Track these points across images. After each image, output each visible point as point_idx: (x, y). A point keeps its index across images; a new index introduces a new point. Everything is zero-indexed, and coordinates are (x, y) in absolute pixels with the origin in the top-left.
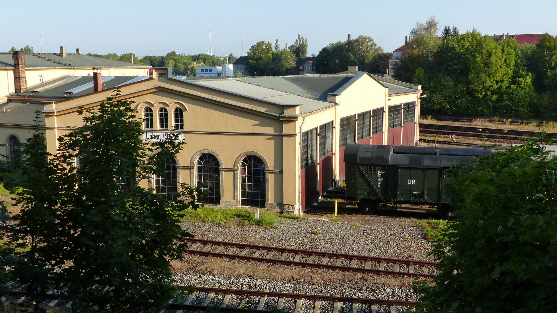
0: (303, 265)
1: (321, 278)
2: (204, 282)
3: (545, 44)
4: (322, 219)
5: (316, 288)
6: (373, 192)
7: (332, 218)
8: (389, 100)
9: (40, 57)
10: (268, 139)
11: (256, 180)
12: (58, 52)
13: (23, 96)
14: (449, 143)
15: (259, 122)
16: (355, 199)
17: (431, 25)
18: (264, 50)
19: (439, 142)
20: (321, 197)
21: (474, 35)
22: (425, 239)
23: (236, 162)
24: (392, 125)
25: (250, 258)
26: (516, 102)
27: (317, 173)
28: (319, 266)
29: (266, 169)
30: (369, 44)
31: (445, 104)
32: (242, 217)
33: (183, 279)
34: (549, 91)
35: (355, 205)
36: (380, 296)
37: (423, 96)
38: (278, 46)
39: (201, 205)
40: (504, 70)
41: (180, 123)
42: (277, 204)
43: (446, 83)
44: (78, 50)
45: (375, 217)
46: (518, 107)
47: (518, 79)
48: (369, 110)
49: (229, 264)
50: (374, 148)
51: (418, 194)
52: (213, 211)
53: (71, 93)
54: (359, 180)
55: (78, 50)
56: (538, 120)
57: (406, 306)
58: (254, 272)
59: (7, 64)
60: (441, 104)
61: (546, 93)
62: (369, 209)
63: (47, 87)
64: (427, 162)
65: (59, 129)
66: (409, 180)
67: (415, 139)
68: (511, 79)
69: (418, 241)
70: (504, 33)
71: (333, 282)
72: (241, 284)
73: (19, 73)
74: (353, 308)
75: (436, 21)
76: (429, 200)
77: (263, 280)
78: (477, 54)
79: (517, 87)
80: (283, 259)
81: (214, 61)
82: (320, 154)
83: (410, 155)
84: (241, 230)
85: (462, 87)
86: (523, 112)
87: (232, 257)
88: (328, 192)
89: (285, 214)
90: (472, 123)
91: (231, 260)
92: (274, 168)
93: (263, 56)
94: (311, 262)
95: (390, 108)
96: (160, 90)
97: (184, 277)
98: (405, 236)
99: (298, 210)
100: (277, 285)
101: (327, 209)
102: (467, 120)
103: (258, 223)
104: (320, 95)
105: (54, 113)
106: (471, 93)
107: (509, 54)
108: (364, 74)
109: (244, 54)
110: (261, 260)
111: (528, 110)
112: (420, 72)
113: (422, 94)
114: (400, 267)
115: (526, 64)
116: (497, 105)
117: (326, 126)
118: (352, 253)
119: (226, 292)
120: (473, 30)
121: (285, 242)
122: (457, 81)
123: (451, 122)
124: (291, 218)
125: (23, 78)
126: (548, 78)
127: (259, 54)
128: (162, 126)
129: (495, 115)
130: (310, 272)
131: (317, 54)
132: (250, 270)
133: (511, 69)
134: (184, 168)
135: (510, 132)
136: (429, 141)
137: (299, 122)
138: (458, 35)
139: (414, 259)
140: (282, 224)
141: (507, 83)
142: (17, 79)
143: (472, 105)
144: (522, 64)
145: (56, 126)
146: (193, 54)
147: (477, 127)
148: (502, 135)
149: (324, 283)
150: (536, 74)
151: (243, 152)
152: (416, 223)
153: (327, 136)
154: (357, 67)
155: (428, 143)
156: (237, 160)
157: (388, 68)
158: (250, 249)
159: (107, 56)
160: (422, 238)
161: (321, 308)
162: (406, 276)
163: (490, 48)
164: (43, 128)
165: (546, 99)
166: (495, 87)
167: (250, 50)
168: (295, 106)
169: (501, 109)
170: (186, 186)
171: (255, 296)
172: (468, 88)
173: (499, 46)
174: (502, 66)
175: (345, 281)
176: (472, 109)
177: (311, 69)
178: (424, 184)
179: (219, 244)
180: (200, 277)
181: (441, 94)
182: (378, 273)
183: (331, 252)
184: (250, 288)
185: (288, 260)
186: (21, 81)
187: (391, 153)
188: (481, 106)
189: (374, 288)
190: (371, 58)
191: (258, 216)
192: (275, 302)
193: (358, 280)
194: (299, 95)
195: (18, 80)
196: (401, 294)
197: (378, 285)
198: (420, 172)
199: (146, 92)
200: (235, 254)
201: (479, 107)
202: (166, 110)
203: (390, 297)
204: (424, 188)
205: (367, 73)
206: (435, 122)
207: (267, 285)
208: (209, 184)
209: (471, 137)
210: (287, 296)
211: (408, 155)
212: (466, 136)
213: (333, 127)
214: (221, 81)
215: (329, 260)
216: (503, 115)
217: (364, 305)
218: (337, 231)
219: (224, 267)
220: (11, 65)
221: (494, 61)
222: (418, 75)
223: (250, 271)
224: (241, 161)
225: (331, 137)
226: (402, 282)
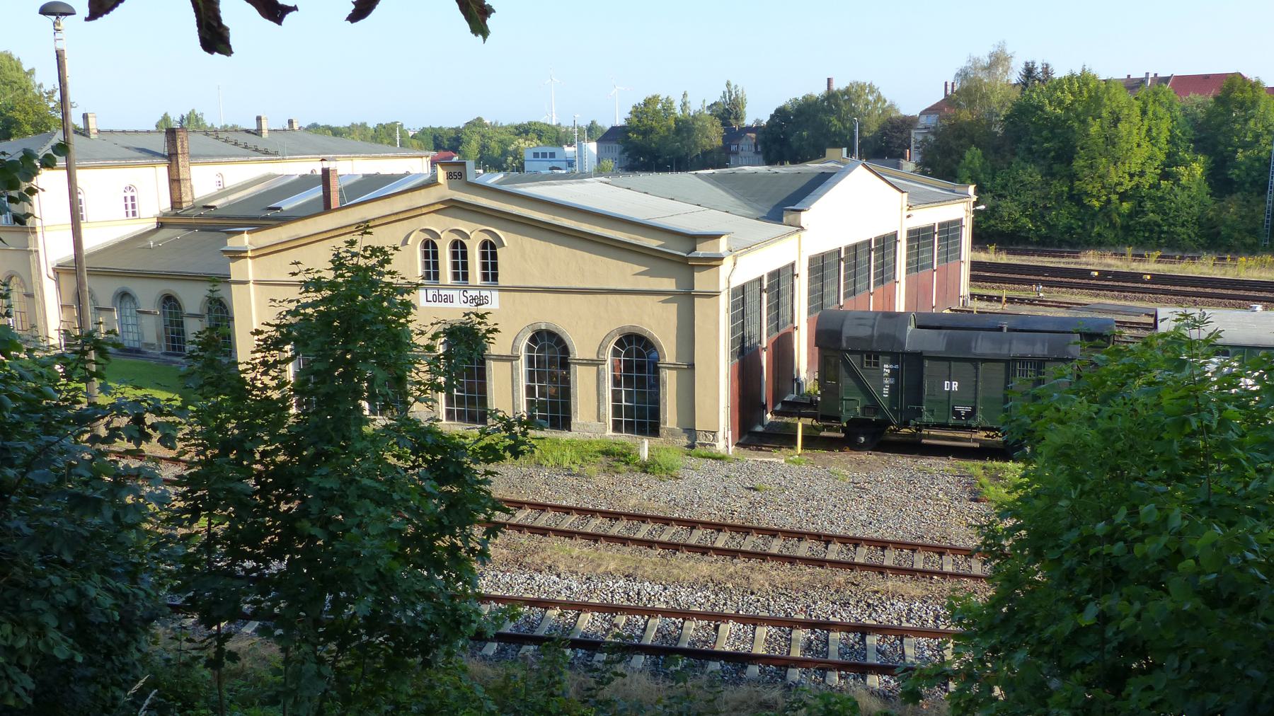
0: (733, 554)
1: (767, 581)
2: (539, 587)
3: (1232, 95)
4: (772, 460)
5: (758, 601)
6: (874, 406)
7: (791, 458)
8: (909, 216)
9: (217, 138)
10: (664, 302)
11: (641, 382)
12: (253, 126)
13: (186, 215)
14: (1031, 302)
16: (838, 419)
17: (998, 60)
18: (659, 112)
19: (1010, 300)
21: (1084, 79)
22: (976, 500)
23: (602, 347)
24: (913, 266)
25: (628, 539)
26: (1171, 215)
28: (763, 556)
29: (662, 361)
30: (870, 98)
31: (1024, 220)
32: (615, 457)
33: (499, 580)
34: (1239, 193)
35: (837, 431)
36: (884, 617)
37: (978, 208)
38: (688, 105)
39: (528, 451)
41: (491, 271)
43: (1026, 178)
44: (291, 122)
46: (1175, 225)
49: (587, 551)
50: (875, 319)
51: (963, 410)
52: (558, 444)
53: (279, 208)
54: (846, 382)
55: (291, 122)
56: (1216, 252)
57: (935, 639)
58: (636, 568)
59: (155, 154)
60: (1015, 221)
61: (1234, 197)
63: (232, 197)
64: (983, 346)
65: (257, 283)
67: (961, 294)
69: (963, 504)
70: (1147, 74)
71: (792, 589)
72: (611, 592)
73: (179, 170)
74: (830, 642)
75: (1009, 52)
77: (653, 583)
78: (1090, 118)
79: (1173, 184)
80: (693, 541)
82: (768, 330)
83: (949, 331)
84: (611, 481)
85: (1060, 186)
86: (1185, 237)
87: (594, 537)
88: (784, 403)
89: (699, 449)
90: (1077, 260)
91: (592, 543)
92: (677, 358)
94: (749, 548)
95: (910, 232)
96: (452, 207)
97: (499, 577)
98: (937, 494)
99: (724, 441)
100: (682, 593)
101: (782, 438)
102: (1068, 252)
103: (645, 468)
104: (768, 210)
105: (246, 252)
106: (1076, 197)
108: (857, 166)
109: (620, 122)
110: (650, 544)
111: (1194, 233)
112: (973, 156)
113: (976, 204)
114: (925, 558)
115: (1193, 138)
116: (1131, 223)
117: (781, 274)
118: (829, 530)
119: (581, 607)
120: (1084, 70)
122: (1050, 174)
123: (1036, 258)
124: (710, 458)
125: (187, 180)
126: (1237, 166)
127: (650, 122)
128: (456, 276)
129: (1126, 243)
130: (747, 567)
131: (765, 119)
132: (629, 563)
133: (1160, 149)
134: (500, 358)
135: (1157, 278)
136: (990, 299)
137: (725, 268)
138: (1052, 80)
139: (954, 543)
140: (692, 469)
141: (1153, 178)
142: (175, 181)
143: (1080, 223)
144: (1185, 138)
145: (251, 277)
146: (517, 122)
147: (1089, 267)
148: (1140, 285)
149: (773, 591)
150: (1212, 158)
151: (615, 326)
152: (959, 468)
153: (781, 292)
154: (845, 150)
155: (987, 303)
156: (604, 345)
157: (909, 147)
158: (629, 520)
159: (349, 128)
160: (971, 500)
161: (766, 640)
162: (935, 577)
163: (1118, 106)
164: (225, 280)
165: (1232, 209)
166: (1128, 185)
167: (631, 113)
169: (1140, 230)
170: (501, 415)
171: (637, 617)
172: (1071, 189)
173: (1137, 102)
175: (814, 588)
176: (1079, 230)
177: (754, 150)
179: (567, 510)
180: (532, 578)
181: (1017, 200)
182: (881, 570)
183: (787, 528)
184: (628, 600)
185: (703, 544)
186: (182, 185)
187: (911, 328)
189: (871, 602)
190: (874, 128)
191: (645, 454)
192: (677, 627)
193: (839, 584)
195: (175, 184)
196: (926, 614)
197: (880, 595)
198: (968, 366)
199: (425, 210)
200: (600, 532)
201: (1093, 226)
202: (463, 246)
203: (903, 619)
204: (976, 398)
205: (864, 165)
206: (1004, 258)
207: (661, 594)
208: (550, 389)
209: (1076, 288)
210: (700, 616)
211: (944, 331)
215: (784, 543)
216: (1142, 243)
217: (851, 636)
218: (801, 484)
219: (578, 557)
220: (163, 156)
222: (971, 162)
223: (629, 566)
224: (612, 345)
225: (790, 293)
226: (928, 590)
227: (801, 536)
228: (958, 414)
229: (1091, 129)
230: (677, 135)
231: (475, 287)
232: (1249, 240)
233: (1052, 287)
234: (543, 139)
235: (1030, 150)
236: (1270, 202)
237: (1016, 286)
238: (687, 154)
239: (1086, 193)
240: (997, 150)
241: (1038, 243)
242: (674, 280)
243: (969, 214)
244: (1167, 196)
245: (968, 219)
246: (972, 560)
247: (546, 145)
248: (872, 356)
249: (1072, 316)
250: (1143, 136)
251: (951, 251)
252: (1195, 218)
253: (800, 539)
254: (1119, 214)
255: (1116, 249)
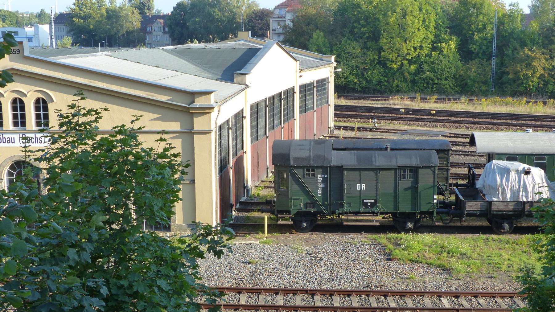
8: (300, 76)
15: (159, 116)
16: (289, 212)
19: (359, 129)
20: (235, 211)
22: (390, 260)
24: (304, 109)
26: (439, 73)
27: (230, 180)
31: (352, 77)
34: (476, 60)
37: (337, 70)
40: (423, 33)
42: (187, 226)
45: (316, 234)
47: (439, 44)
48: (279, 91)
51: (369, 202)
54: (294, 187)
60: (346, 78)
61: (474, 62)
62: (306, 224)
64: (380, 160)
66: (358, 185)
67: (329, 126)
68: (432, 45)
76: (383, 209)
78: (390, 12)
86: (448, 86)
88: (241, 203)
93: (94, 14)
95: (301, 87)
102: (382, 97)
104: (221, 74)
107: (427, 13)
112: (318, 36)
113: (335, 68)
114: (376, 300)
115: (449, 26)
121: (218, 277)
122: (365, 47)
123: (362, 101)
127: (88, 11)
128: (16, 124)
133: (431, 32)
135: (440, 113)
143: (386, 79)
144: (444, 25)
150: (460, 38)
154: (250, 32)
160: (387, 260)
166: (413, 54)
168: (209, 93)
169: (421, 83)
172: (379, 57)
174: (420, 28)
176: (386, 83)
177: (162, 31)
178: (377, 188)
188: (397, 79)
194: (195, 75)
198: (372, 173)
201: (394, 81)
202: (21, 102)
209: (396, 120)
212: (390, 120)
213: (243, 117)
214: (87, 58)
216: (423, 91)
221: (410, 22)
224: (7, 169)
227: (295, 292)
228: (366, 205)
229: (390, 20)
230: (108, 20)
231: (31, 132)
232: (484, 88)
233: (381, 120)
234: (7, 21)
235: (352, 32)
236: (494, 65)
237: (359, 120)
238: (116, 34)
239: (388, 60)
240: (331, 32)
241: (361, 92)
242: (179, 124)
243: (332, 74)
244: (436, 62)
245: (332, 77)
246: (405, 298)
247: (8, 26)
248: (311, 170)
249: (399, 138)
250: (420, 24)
251: (323, 100)
252: (453, 75)
253: (295, 294)
254: (409, 73)
255: (408, 95)
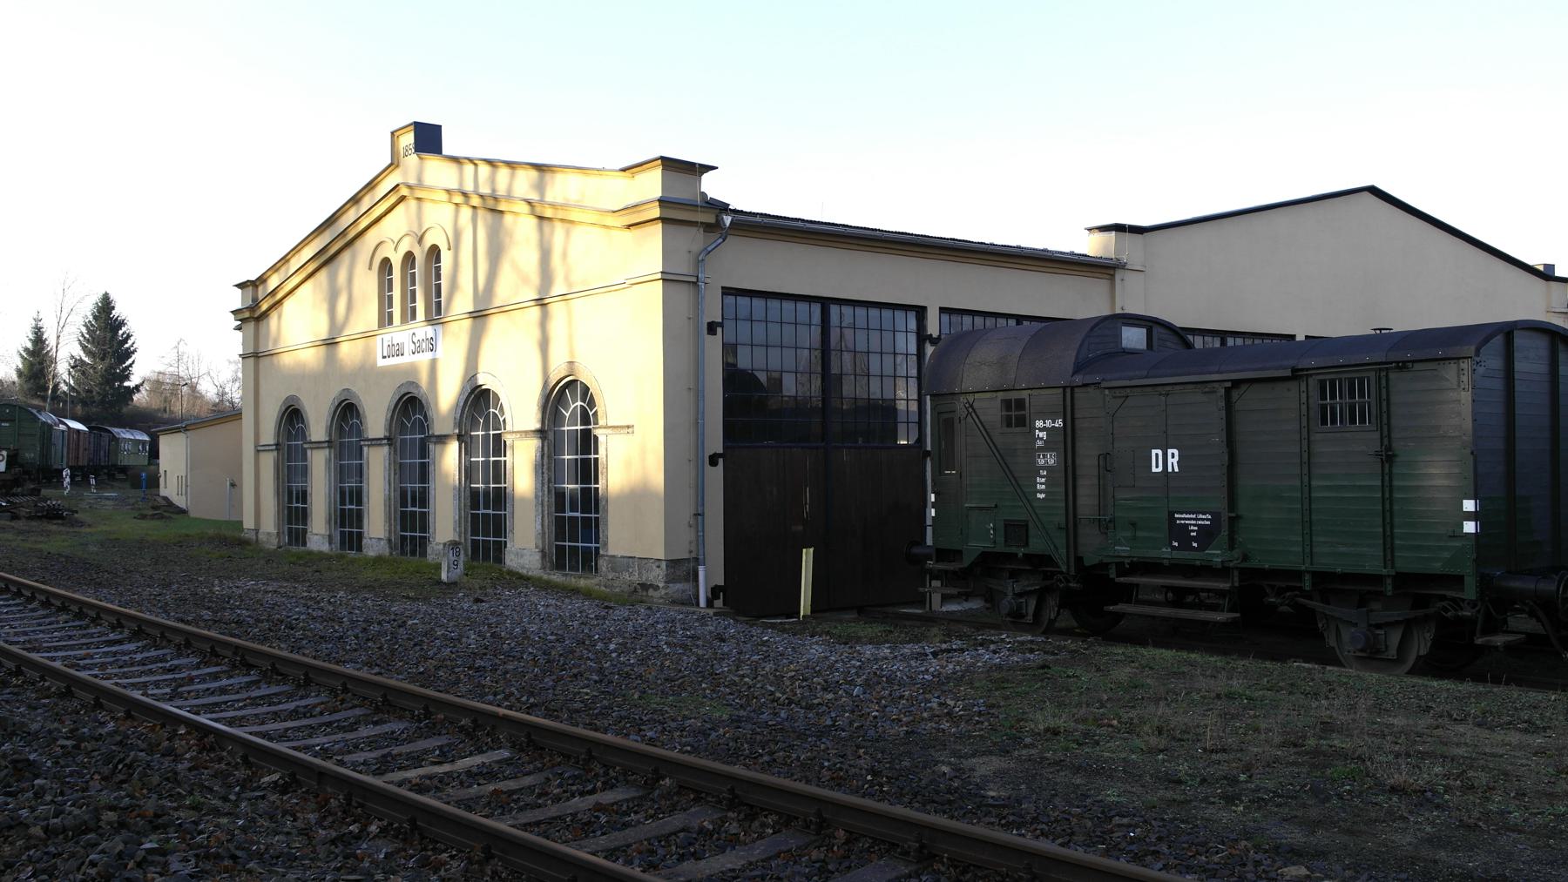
66: (1154, 452)
81: (260, 537)
